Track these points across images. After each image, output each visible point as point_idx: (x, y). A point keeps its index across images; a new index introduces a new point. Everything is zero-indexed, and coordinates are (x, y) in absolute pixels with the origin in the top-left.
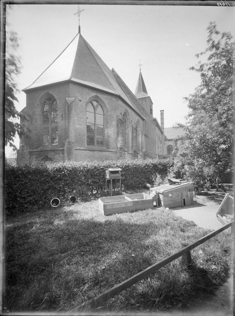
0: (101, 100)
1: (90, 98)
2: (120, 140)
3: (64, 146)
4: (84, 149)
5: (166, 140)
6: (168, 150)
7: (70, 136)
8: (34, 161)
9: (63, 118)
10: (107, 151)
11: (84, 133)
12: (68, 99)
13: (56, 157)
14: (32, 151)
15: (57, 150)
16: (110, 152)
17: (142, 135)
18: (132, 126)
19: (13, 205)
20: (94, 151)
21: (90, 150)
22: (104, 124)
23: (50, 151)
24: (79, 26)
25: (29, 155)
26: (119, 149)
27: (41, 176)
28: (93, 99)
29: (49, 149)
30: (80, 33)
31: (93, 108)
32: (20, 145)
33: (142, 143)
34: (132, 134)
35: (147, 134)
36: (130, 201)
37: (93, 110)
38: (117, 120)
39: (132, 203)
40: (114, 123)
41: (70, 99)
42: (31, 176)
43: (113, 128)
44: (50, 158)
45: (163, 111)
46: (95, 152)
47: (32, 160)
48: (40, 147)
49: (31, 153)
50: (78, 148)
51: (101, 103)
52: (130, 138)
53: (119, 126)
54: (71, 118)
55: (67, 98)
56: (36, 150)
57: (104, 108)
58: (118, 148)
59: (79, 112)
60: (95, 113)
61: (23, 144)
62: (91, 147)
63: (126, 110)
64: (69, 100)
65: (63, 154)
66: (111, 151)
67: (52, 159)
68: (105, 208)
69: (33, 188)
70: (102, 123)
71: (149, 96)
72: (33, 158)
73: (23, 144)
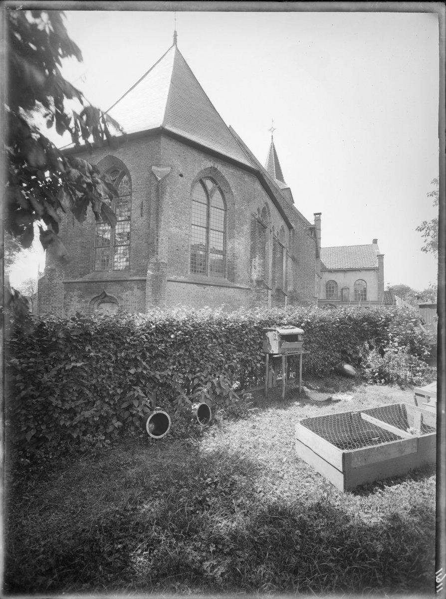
0: (223, 177)
1: (201, 171)
2: (257, 264)
3: (144, 271)
4: (186, 280)
5: (325, 270)
6: (327, 291)
7: (159, 250)
8: (75, 303)
9: (143, 212)
11: (187, 246)
12: (157, 170)
13: (124, 297)
14: (73, 281)
15: (127, 281)
16: (237, 290)
17: (287, 258)
18: (274, 238)
19: (39, 431)
20: (205, 286)
21: (198, 282)
22: (225, 227)
23: (112, 281)
24: (175, 32)
25: (65, 289)
26: (255, 284)
27: (118, 346)
28: (206, 176)
29: (109, 279)
30: (176, 45)
31: (204, 194)
32: (46, 266)
33: (286, 273)
34: (274, 254)
35: (296, 256)
36: (410, 438)
37: (205, 199)
38: (253, 222)
39: (415, 445)
40: (246, 228)
41: (162, 169)
42: (91, 345)
43: (243, 239)
44: (112, 298)
45: (320, 214)
46: (208, 288)
47: (71, 300)
48: (89, 273)
49: (68, 286)
50: (173, 278)
51: (220, 184)
53: (257, 234)
54: (162, 211)
55: (154, 168)
56: (80, 280)
58: (252, 281)
59: (177, 198)
60: (208, 205)
61: (53, 266)
62: (199, 277)
63: (266, 204)
64: (160, 171)
65: (143, 289)
66: (238, 288)
67: (116, 299)
68: (346, 465)
69: (94, 382)
70: (223, 227)
71: (288, 187)
72: (72, 297)
73: (53, 266)
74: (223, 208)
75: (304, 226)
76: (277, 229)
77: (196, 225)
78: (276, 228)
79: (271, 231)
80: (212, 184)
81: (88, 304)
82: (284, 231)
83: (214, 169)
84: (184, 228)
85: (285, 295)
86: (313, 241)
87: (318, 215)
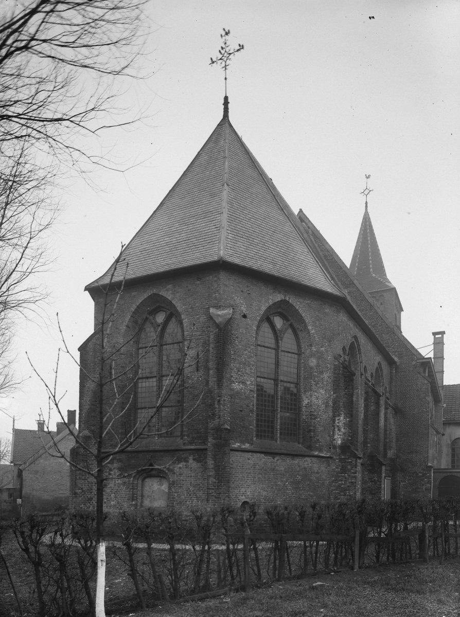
4: (252, 448)
10: (308, 456)
15: (181, 450)
17: (386, 408)
18: (366, 383)
24: (226, 98)
29: (157, 448)
31: (271, 335)
37: (273, 341)
41: (222, 312)
43: (323, 392)
44: (160, 471)
45: (443, 333)
47: (110, 474)
50: (237, 445)
52: (362, 416)
55: (212, 310)
57: (301, 335)
58: (335, 447)
60: (277, 349)
63: (355, 337)
72: (111, 470)
74: (296, 352)
75: (412, 361)
76: (372, 369)
77: (262, 378)
78: (369, 368)
79: (362, 375)
80: (282, 320)
81: (132, 479)
82: (381, 370)
83: (284, 302)
84: (248, 383)
85: (381, 464)
86: (426, 382)
87: (439, 340)
